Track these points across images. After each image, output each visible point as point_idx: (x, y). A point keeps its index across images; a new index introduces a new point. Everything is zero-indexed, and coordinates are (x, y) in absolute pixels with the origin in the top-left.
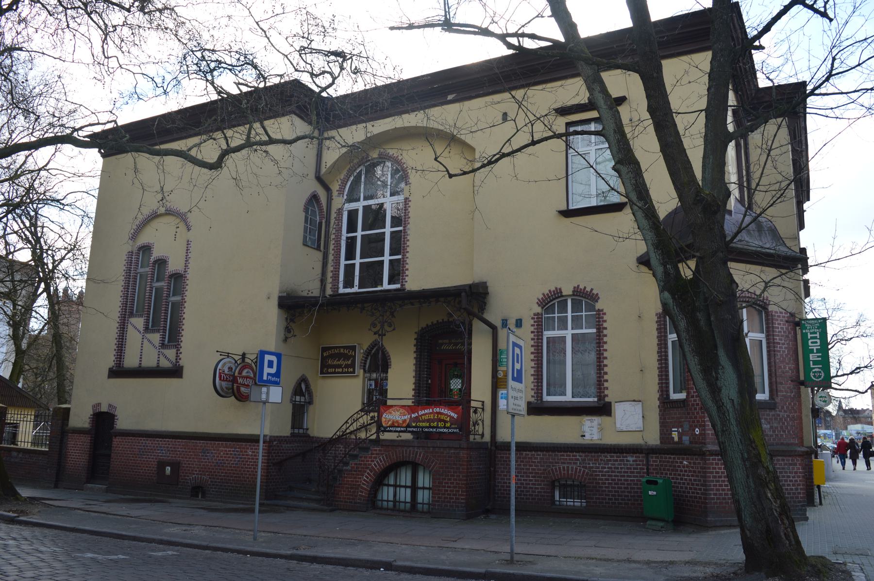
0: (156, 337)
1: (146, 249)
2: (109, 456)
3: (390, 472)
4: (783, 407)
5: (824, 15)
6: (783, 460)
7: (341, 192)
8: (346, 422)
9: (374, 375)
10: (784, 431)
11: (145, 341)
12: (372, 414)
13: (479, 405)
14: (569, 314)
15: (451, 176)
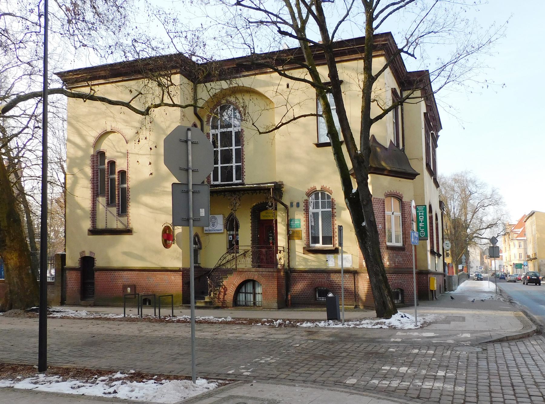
0: (114, 210)
1: (102, 154)
2: (93, 284)
3: (243, 286)
4: (408, 250)
5: (413, 56)
6: (408, 276)
7: (208, 121)
8: (220, 259)
9: (231, 233)
10: (409, 262)
11: (108, 212)
12: (232, 254)
13: (282, 249)
14: (320, 200)
15: (260, 133)
